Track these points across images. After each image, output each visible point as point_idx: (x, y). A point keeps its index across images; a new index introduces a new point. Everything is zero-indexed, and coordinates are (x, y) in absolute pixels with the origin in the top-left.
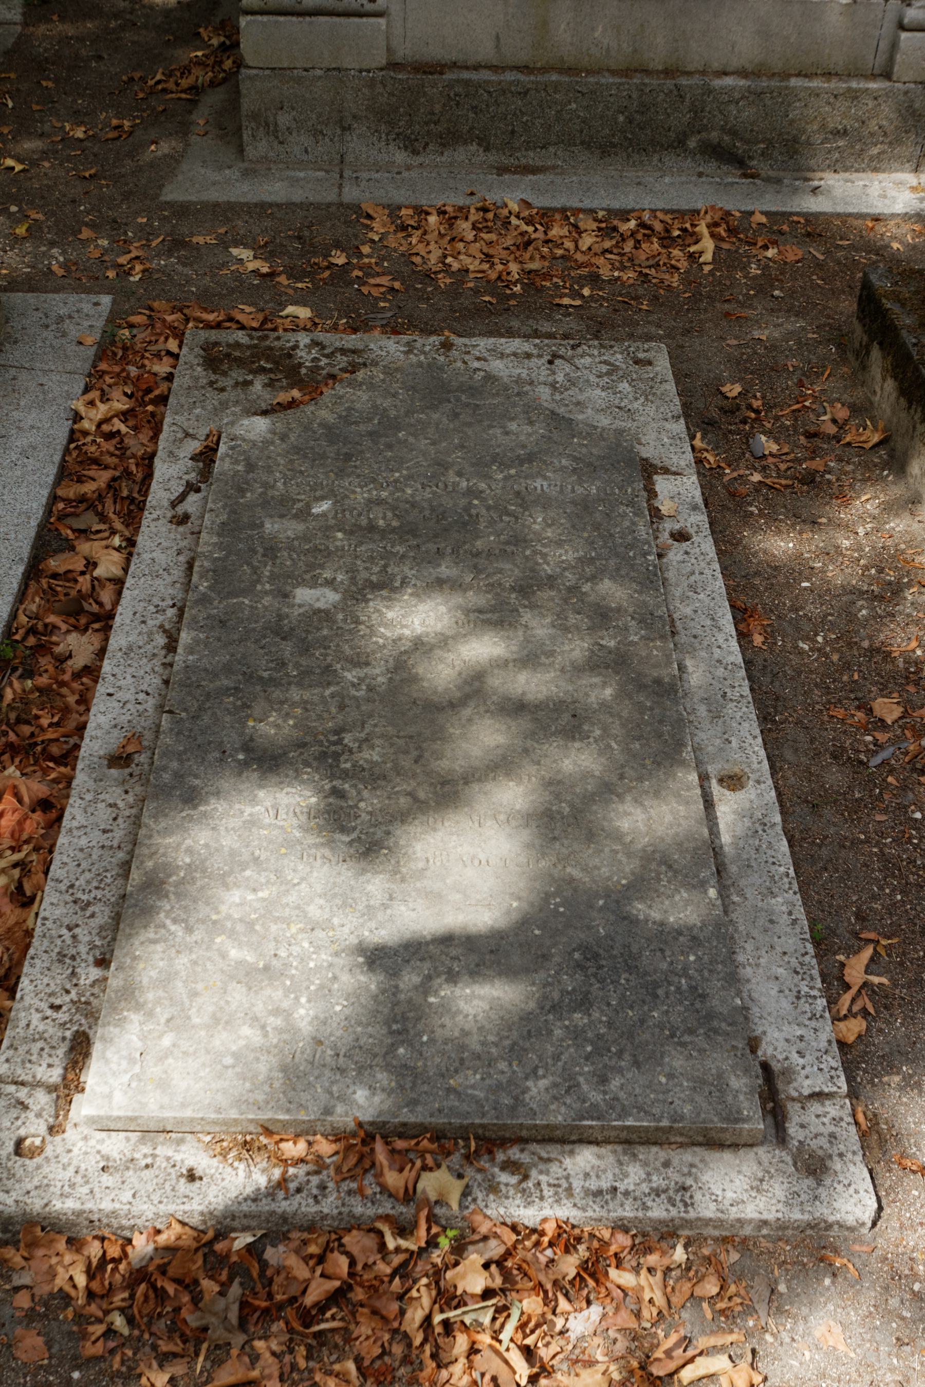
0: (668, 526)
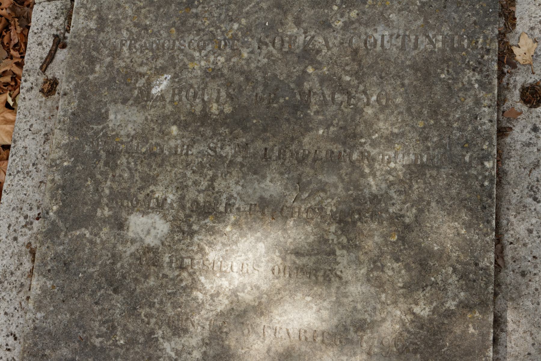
0: (520, 79)
